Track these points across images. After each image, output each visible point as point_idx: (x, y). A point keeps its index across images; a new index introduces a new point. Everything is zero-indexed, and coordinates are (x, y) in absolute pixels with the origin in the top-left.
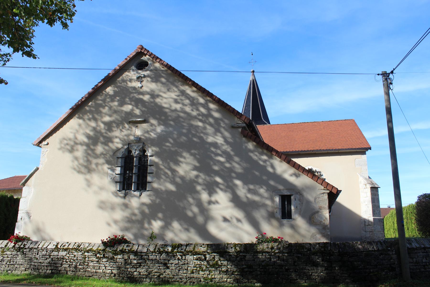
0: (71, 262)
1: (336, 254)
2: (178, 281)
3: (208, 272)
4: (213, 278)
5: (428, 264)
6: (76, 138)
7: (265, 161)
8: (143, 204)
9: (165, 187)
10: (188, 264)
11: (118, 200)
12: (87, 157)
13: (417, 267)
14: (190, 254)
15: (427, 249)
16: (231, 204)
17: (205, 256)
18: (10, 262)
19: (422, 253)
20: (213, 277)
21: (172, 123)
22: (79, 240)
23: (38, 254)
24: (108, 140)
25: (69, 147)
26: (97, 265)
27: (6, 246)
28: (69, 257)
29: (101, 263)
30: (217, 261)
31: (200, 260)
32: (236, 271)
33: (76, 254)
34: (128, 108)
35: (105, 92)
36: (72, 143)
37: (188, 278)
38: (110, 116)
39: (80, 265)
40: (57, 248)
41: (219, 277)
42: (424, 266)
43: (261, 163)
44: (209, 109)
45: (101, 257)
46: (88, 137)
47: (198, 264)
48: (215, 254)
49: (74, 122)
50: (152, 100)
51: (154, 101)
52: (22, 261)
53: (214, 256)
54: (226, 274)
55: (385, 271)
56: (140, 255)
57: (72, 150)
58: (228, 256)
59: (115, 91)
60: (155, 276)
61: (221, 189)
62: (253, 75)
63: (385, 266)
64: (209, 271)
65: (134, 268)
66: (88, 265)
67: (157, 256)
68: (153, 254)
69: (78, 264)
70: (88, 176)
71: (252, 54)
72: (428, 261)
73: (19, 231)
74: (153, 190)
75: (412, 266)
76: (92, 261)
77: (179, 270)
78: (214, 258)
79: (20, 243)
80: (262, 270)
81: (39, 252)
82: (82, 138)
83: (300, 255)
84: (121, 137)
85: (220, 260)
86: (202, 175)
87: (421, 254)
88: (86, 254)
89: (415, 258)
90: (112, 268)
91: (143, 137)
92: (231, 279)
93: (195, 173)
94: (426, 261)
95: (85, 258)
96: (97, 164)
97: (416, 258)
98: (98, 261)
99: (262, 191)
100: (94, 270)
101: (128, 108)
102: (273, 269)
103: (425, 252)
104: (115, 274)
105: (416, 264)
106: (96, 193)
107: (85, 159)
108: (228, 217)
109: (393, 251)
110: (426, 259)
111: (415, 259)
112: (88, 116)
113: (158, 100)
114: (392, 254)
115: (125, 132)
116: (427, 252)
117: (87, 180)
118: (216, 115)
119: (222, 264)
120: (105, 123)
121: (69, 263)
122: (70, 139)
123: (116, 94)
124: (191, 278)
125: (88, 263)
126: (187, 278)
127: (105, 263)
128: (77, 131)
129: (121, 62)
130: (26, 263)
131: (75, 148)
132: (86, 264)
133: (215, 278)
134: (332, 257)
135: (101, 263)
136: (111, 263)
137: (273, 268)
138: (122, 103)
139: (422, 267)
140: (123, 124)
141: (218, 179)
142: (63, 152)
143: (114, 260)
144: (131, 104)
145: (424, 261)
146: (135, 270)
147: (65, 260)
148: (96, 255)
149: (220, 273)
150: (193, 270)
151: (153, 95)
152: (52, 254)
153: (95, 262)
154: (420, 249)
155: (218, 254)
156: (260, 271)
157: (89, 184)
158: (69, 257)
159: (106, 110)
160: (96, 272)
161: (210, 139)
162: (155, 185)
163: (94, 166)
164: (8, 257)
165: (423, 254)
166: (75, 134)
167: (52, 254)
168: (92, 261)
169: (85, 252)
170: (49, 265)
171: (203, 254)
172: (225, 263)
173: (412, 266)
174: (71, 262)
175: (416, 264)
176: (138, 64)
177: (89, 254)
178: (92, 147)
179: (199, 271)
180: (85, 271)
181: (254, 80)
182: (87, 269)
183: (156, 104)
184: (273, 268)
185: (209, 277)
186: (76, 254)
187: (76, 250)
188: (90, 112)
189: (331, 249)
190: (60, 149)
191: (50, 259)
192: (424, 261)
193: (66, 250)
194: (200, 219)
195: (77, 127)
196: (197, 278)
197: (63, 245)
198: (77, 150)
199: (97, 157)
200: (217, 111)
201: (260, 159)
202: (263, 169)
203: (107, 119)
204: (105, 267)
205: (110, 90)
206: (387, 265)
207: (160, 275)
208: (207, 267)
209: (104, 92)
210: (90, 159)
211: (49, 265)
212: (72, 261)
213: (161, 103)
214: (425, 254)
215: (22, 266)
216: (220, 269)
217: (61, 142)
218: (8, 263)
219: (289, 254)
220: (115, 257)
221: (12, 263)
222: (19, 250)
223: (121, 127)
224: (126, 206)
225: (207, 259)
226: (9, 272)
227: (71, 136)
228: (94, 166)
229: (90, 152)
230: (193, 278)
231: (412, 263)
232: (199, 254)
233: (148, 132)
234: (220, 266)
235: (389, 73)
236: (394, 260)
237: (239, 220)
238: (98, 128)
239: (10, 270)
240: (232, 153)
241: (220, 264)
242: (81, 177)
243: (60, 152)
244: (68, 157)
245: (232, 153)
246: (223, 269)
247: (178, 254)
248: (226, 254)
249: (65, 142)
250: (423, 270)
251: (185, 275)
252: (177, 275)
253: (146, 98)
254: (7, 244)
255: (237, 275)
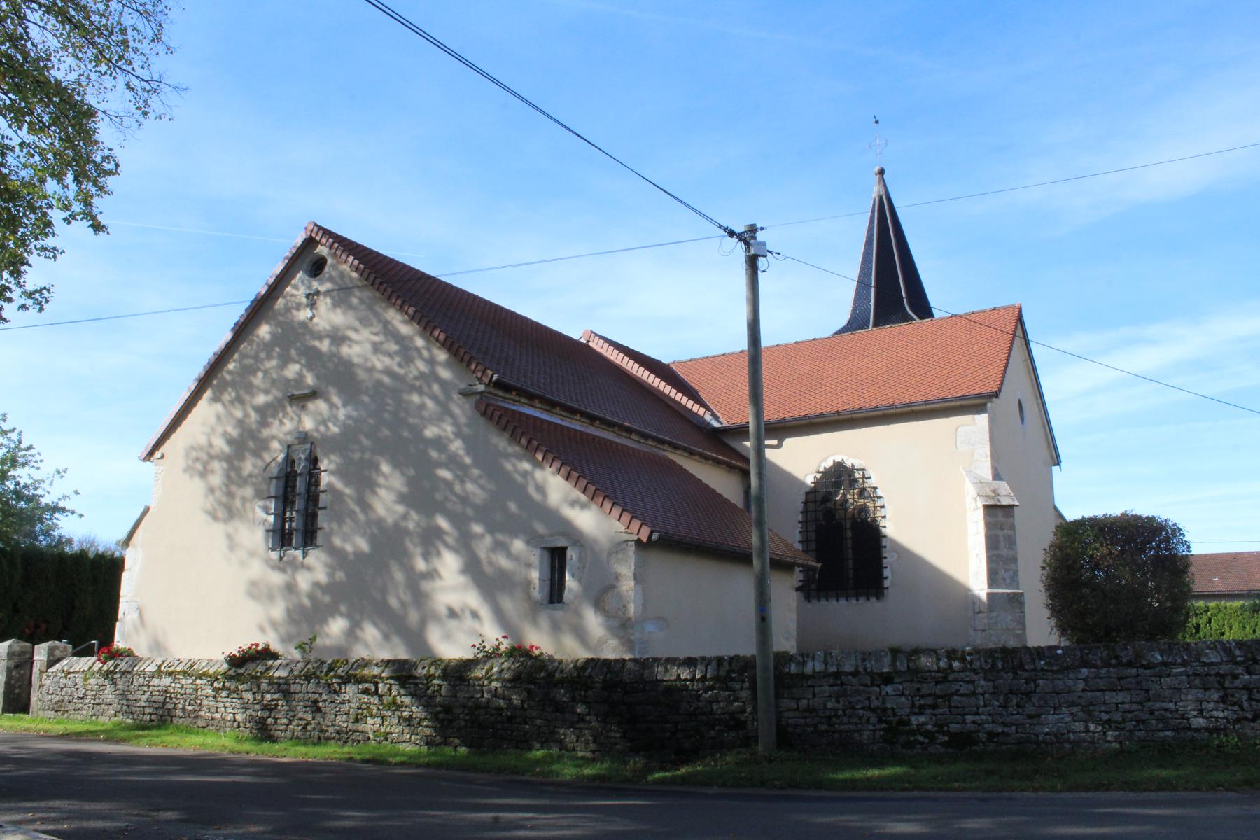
0: (177, 699)
1: (597, 685)
2: (334, 738)
3: (379, 720)
4: (388, 734)
5: (840, 713)
6: (211, 445)
7: (525, 474)
8: (317, 585)
9: (354, 545)
10: (349, 702)
11: (277, 579)
12: (227, 486)
13: (808, 720)
14: (353, 681)
15: (843, 677)
16: (462, 579)
17: (376, 684)
18: (95, 700)
19: (830, 686)
20: (388, 729)
21: (366, 399)
22: (195, 655)
23: (132, 684)
24: (263, 445)
25: (199, 466)
26: (213, 703)
27: (90, 668)
28: (174, 689)
29: (219, 699)
30: (395, 696)
31: (369, 694)
32: (425, 719)
33: (183, 681)
34: (292, 370)
35: (258, 336)
36: (204, 456)
37: (350, 731)
38: (266, 392)
39: (189, 705)
40: (159, 673)
41: (397, 731)
42: (830, 718)
43: (518, 478)
44: (432, 362)
45: (219, 689)
46: (230, 441)
47: (365, 703)
48: (392, 682)
49: (205, 409)
50: (334, 349)
51: (339, 352)
52: (110, 696)
53: (391, 685)
54: (409, 725)
55: (717, 728)
56: (277, 683)
57: (204, 474)
58: (412, 686)
59: (272, 334)
60: (300, 728)
61: (448, 547)
62: (879, 183)
63: (717, 716)
64: (382, 718)
65: (268, 709)
66: (200, 704)
67: (302, 685)
68: (297, 681)
69: (187, 704)
70: (230, 528)
71: (877, 122)
72: (840, 706)
73: (119, 642)
74: (334, 552)
75: (794, 718)
76: (207, 697)
77: (336, 716)
78: (390, 689)
79: (111, 663)
80: (468, 718)
81: (135, 680)
82: (220, 445)
83: (533, 687)
84: (281, 436)
85: (399, 693)
86: (414, 516)
87: (826, 688)
88: (198, 681)
89: (804, 698)
90: (235, 711)
91: (315, 434)
92: (418, 737)
93: (400, 509)
94: (837, 705)
95: (197, 690)
96: (244, 500)
97: (809, 699)
98: (215, 697)
99: (518, 545)
100: (209, 715)
101: (292, 370)
102: (487, 717)
103: (837, 685)
104: (239, 723)
105: (808, 714)
106: (243, 564)
107: (224, 489)
108: (457, 608)
109: (743, 681)
110: (838, 702)
111: (804, 703)
112: (230, 394)
113: (345, 350)
114: (742, 689)
115: (288, 425)
116: (842, 684)
117: (230, 537)
118: (445, 374)
119: (402, 702)
120: (258, 409)
121: (174, 700)
122: (201, 448)
123: (276, 340)
124: (354, 731)
125: (201, 700)
126: (347, 733)
127: (225, 700)
128: (213, 430)
129: (279, 268)
130: (116, 701)
131: (209, 468)
132: (199, 702)
133: (392, 733)
134: (591, 692)
135: (219, 699)
136: (234, 700)
137: (486, 714)
138: (285, 361)
139: (823, 720)
140: (284, 407)
141: (443, 523)
142: (191, 476)
143: (238, 694)
144: (298, 362)
145: (829, 707)
146: (268, 713)
147: (168, 695)
148: (212, 684)
149: (399, 722)
150: (357, 715)
151: (338, 338)
152: (151, 684)
153: (211, 699)
154: (824, 677)
155: (396, 680)
156: (466, 721)
157: (232, 543)
158: (174, 689)
159: (258, 379)
160: (212, 719)
161: (430, 432)
162: (337, 542)
163: (238, 503)
164: (92, 690)
165: (832, 689)
166: (209, 436)
167: (151, 684)
168: (207, 697)
169: (196, 679)
170: (147, 704)
171: (375, 680)
172: (407, 700)
173: (794, 718)
174: (177, 699)
175: (808, 714)
176: (313, 265)
177: (202, 682)
178: (236, 463)
179: (367, 717)
180: (196, 717)
181: (884, 197)
182: (201, 713)
183: (341, 359)
184: (486, 714)
185: (383, 730)
186: (183, 681)
187: (185, 673)
188: (233, 384)
189: (593, 674)
190: (186, 470)
191: (149, 693)
192: (829, 705)
193: (170, 674)
194: (413, 617)
195: (213, 420)
196: (363, 732)
197: (165, 665)
198: (213, 472)
199: (243, 482)
200: (447, 365)
201: (516, 471)
202: (520, 493)
203: (261, 399)
204: (226, 708)
205: (264, 331)
206: (724, 714)
207: (307, 724)
208: (378, 709)
209: (255, 339)
210: (233, 488)
211: (147, 704)
212: (179, 696)
213: (349, 356)
214: (836, 688)
215: (111, 707)
216: (399, 713)
217: (187, 455)
218: (92, 702)
219: (513, 684)
220: (240, 687)
221: (97, 701)
222: (108, 675)
223: (281, 415)
224: (290, 588)
225: (380, 691)
226: (94, 718)
227: (203, 440)
228: (238, 503)
229: (233, 474)
230: (358, 731)
231: (795, 710)
232: (366, 681)
233: (324, 422)
234: (399, 707)
235: (740, 240)
236: (744, 702)
237: (475, 615)
238: (247, 421)
239: (94, 715)
240: (468, 460)
241: (399, 703)
242: (219, 529)
243: (187, 476)
244: (198, 485)
245: (468, 460)
246: (405, 714)
247: (334, 681)
248: (411, 681)
249: (194, 454)
250: (824, 727)
251: (345, 725)
252: (332, 725)
253: (325, 346)
254: (94, 664)
255: (427, 727)
